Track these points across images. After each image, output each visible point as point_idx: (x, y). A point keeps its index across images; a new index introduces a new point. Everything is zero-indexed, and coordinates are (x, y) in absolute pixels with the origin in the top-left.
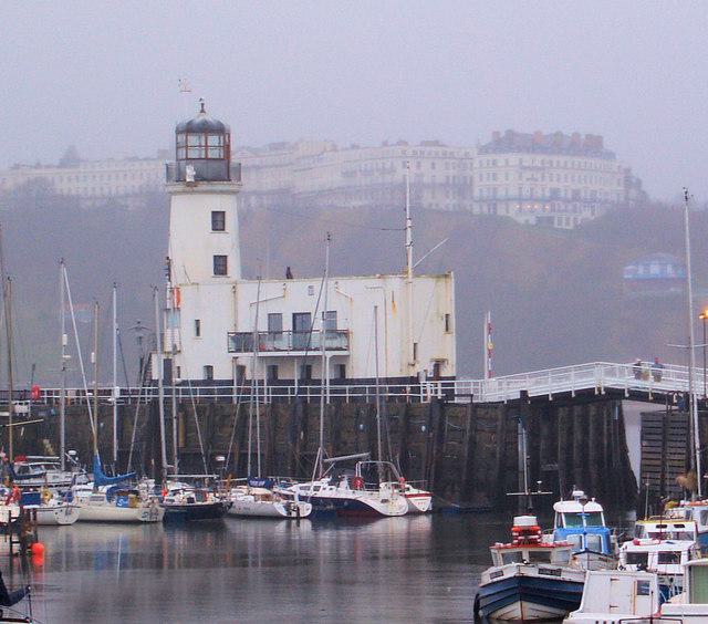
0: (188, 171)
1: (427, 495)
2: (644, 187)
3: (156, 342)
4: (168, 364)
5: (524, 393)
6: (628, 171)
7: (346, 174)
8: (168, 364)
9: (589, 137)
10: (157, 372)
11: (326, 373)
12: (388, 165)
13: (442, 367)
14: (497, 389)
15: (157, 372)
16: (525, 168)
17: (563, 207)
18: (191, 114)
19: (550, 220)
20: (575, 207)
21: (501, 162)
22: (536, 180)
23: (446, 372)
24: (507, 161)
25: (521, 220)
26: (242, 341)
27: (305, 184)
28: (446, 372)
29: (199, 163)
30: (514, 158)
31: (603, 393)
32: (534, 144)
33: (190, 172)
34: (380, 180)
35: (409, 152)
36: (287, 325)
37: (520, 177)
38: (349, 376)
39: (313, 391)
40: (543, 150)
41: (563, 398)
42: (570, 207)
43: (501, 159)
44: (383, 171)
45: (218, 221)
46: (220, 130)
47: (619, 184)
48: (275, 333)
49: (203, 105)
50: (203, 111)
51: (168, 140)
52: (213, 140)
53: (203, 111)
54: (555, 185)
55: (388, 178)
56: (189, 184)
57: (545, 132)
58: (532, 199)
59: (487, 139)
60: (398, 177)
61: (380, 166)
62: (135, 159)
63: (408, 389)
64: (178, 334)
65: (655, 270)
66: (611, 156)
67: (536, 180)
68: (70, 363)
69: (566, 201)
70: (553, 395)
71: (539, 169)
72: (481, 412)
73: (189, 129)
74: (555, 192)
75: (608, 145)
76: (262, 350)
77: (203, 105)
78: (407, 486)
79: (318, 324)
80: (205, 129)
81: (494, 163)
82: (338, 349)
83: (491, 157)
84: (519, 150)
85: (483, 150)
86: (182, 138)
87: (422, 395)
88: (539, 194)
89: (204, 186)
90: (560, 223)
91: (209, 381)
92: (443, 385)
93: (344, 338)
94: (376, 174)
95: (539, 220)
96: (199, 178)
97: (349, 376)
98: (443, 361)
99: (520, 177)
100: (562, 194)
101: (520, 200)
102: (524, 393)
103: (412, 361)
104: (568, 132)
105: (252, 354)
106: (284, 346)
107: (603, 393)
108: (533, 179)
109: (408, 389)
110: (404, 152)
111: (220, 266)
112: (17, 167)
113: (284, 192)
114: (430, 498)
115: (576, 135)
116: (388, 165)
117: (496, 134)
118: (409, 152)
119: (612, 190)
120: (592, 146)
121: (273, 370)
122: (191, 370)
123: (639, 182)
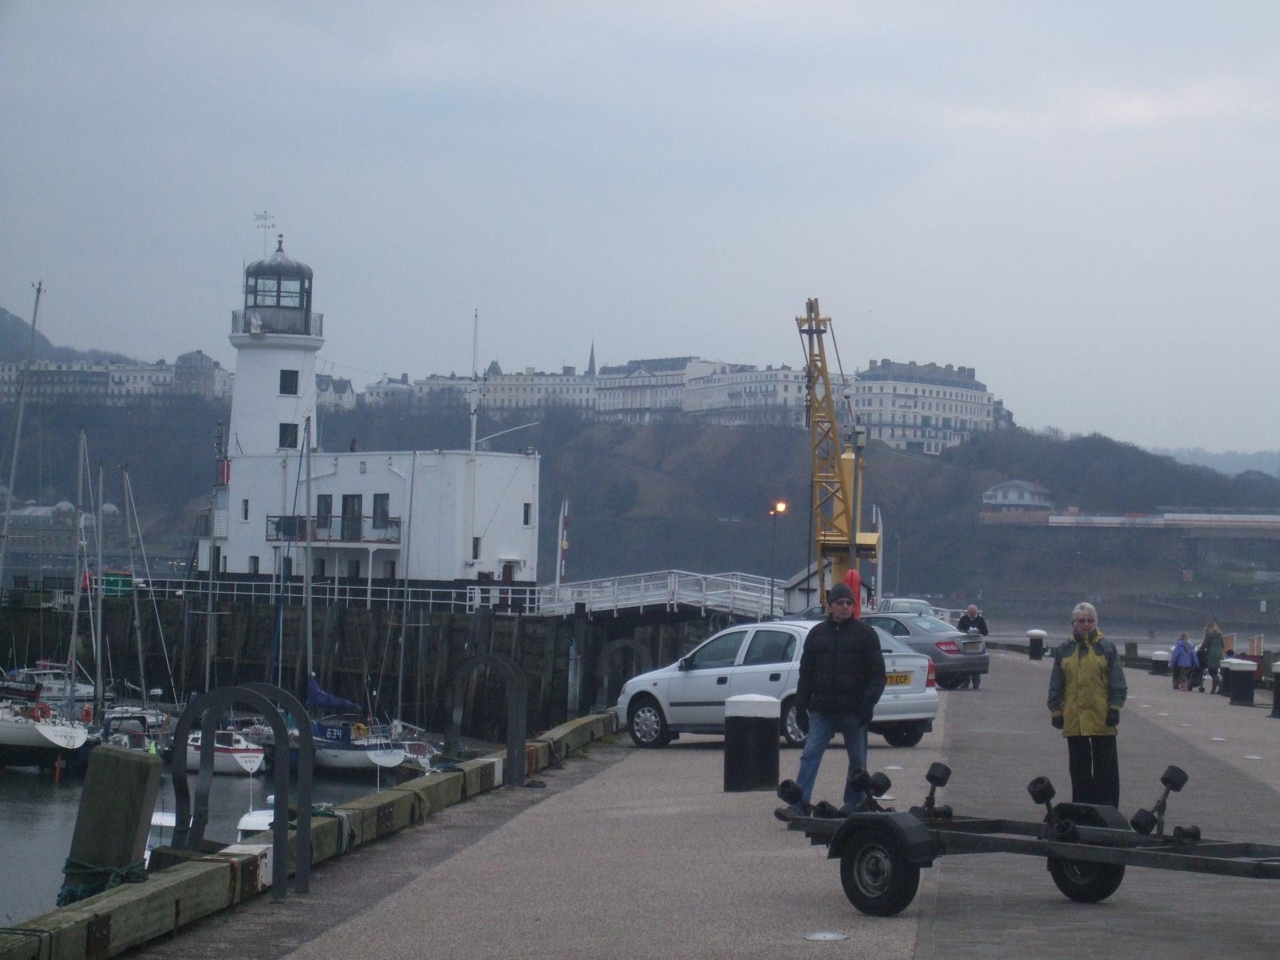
0: (253, 320)
1: (254, 751)
2: (1015, 419)
3: (205, 527)
4: (216, 552)
5: (580, 607)
6: (1000, 403)
7: (731, 395)
8: (216, 552)
9: (962, 369)
10: (204, 564)
11: (370, 572)
12: (771, 388)
13: (516, 569)
14: (559, 600)
15: (204, 564)
16: (900, 396)
17: (933, 434)
18: (266, 255)
19: (920, 445)
20: (945, 434)
21: (876, 390)
22: (909, 407)
23: (519, 576)
24: (882, 389)
25: (892, 444)
26: (289, 527)
27: (693, 402)
28: (519, 576)
29: (268, 313)
30: (888, 386)
31: (676, 610)
32: (910, 373)
33: (256, 321)
34: (763, 402)
35: (791, 378)
36: (337, 509)
37: (894, 404)
38: (400, 575)
39: (259, 588)
40: (922, 380)
41: (630, 616)
42: (940, 434)
43: (876, 386)
44: (766, 394)
45: (289, 382)
46: (302, 274)
47: (988, 415)
48: (324, 517)
49: (280, 242)
50: (280, 250)
51: (240, 280)
52: (292, 286)
53: (280, 250)
54: (926, 413)
55: (770, 401)
56: (255, 336)
57: (920, 363)
58: (904, 426)
59: (864, 367)
60: (780, 400)
61: (764, 389)
62: (542, 374)
63: (454, 596)
64: (226, 521)
65: (1013, 497)
66: (982, 387)
67: (909, 407)
68: (90, 541)
69: (936, 428)
70: (619, 610)
71: (910, 397)
72: (529, 628)
73: (257, 272)
74: (926, 420)
75: (979, 377)
76: (315, 539)
77: (280, 242)
78: (238, 737)
79: (367, 508)
80: (279, 271)
81: (870, 389)
82: (388, 541)
83: (868, 384)
84: (896, 378)
85: (862, 377)
86: (252, 282)
87: (468, 603)
88: (910, 421)
89: (272, 338)
90: (929, 449)
91: (289, 576)
92: (513, 592)
93: (394, 527)
94: (760, 396)
95: (909, 445)
96: (267, 327)
97: (400, 575)
98: (518, 563)
99: (894, 404)
100: (933, 422)
101: (893, 426)
102: (580, 607)
103: (470, 559)
104: (942, 364)
105: (303, 544)
106: (332, 537)
107: (676, 610)
108: (905, 406)
109: (454, 596)
110: (786, 376)
111: (288, 434)
112: (433, 377)
113: (673, 410)
114: (261, 756)
115: (950, 367)
116: (771, 388)
117: (872, 363)
118: (791, 378)
119: (983, 420)
120: (964, 378)
121: (320, 565)
122: (237, 564)
123: (1010, 415)
